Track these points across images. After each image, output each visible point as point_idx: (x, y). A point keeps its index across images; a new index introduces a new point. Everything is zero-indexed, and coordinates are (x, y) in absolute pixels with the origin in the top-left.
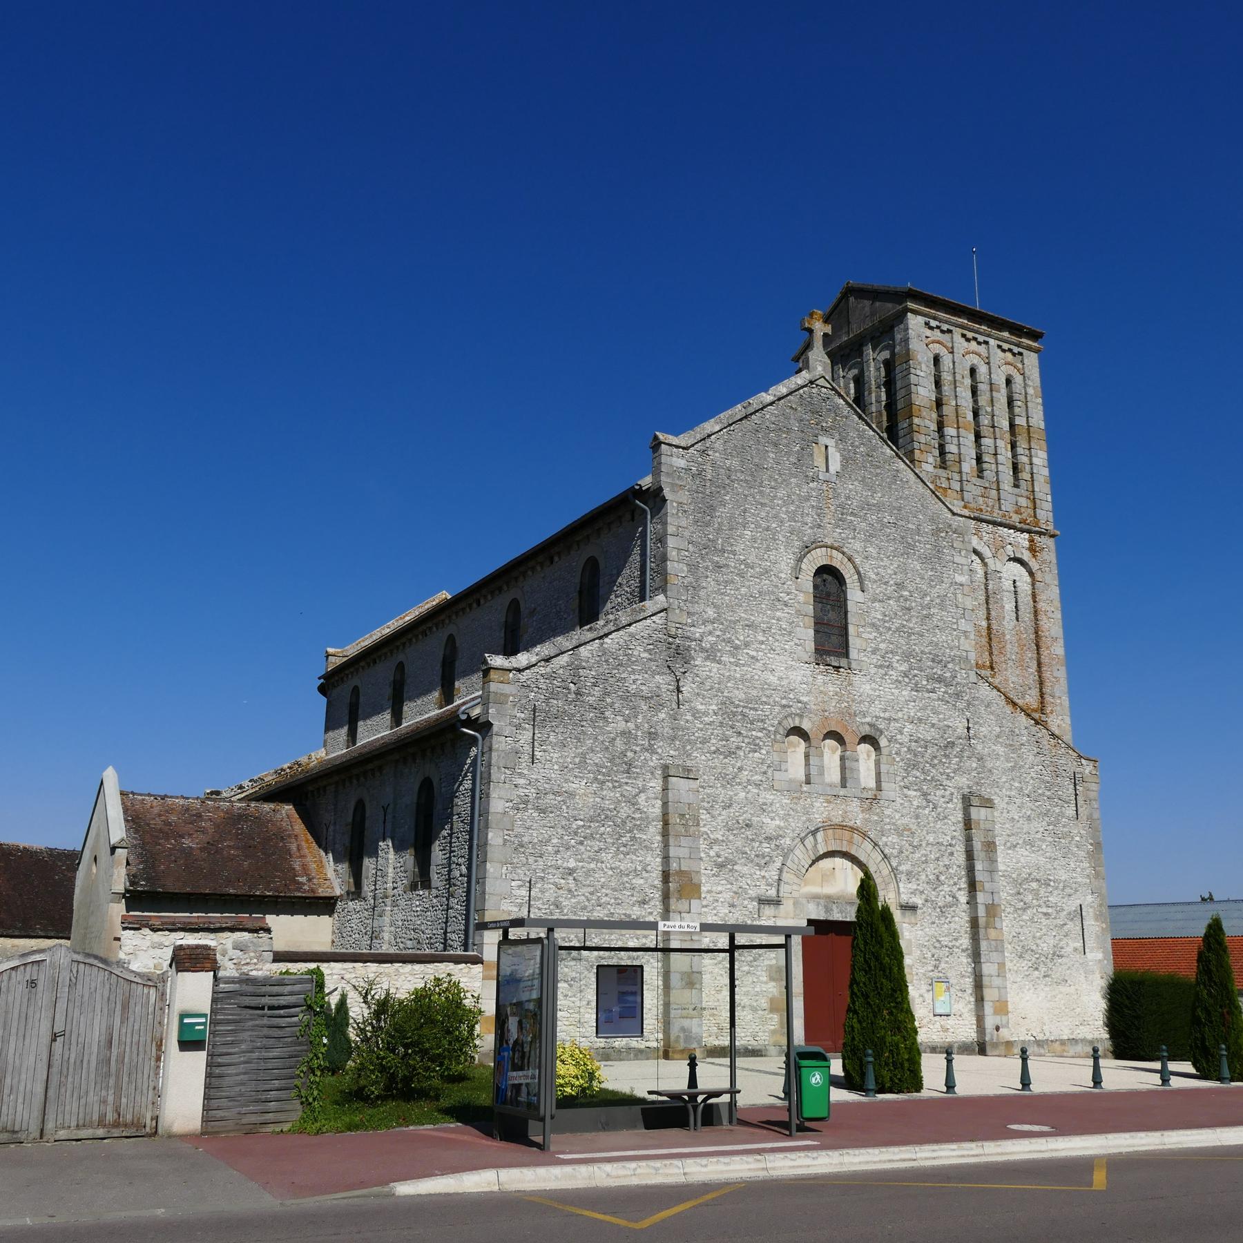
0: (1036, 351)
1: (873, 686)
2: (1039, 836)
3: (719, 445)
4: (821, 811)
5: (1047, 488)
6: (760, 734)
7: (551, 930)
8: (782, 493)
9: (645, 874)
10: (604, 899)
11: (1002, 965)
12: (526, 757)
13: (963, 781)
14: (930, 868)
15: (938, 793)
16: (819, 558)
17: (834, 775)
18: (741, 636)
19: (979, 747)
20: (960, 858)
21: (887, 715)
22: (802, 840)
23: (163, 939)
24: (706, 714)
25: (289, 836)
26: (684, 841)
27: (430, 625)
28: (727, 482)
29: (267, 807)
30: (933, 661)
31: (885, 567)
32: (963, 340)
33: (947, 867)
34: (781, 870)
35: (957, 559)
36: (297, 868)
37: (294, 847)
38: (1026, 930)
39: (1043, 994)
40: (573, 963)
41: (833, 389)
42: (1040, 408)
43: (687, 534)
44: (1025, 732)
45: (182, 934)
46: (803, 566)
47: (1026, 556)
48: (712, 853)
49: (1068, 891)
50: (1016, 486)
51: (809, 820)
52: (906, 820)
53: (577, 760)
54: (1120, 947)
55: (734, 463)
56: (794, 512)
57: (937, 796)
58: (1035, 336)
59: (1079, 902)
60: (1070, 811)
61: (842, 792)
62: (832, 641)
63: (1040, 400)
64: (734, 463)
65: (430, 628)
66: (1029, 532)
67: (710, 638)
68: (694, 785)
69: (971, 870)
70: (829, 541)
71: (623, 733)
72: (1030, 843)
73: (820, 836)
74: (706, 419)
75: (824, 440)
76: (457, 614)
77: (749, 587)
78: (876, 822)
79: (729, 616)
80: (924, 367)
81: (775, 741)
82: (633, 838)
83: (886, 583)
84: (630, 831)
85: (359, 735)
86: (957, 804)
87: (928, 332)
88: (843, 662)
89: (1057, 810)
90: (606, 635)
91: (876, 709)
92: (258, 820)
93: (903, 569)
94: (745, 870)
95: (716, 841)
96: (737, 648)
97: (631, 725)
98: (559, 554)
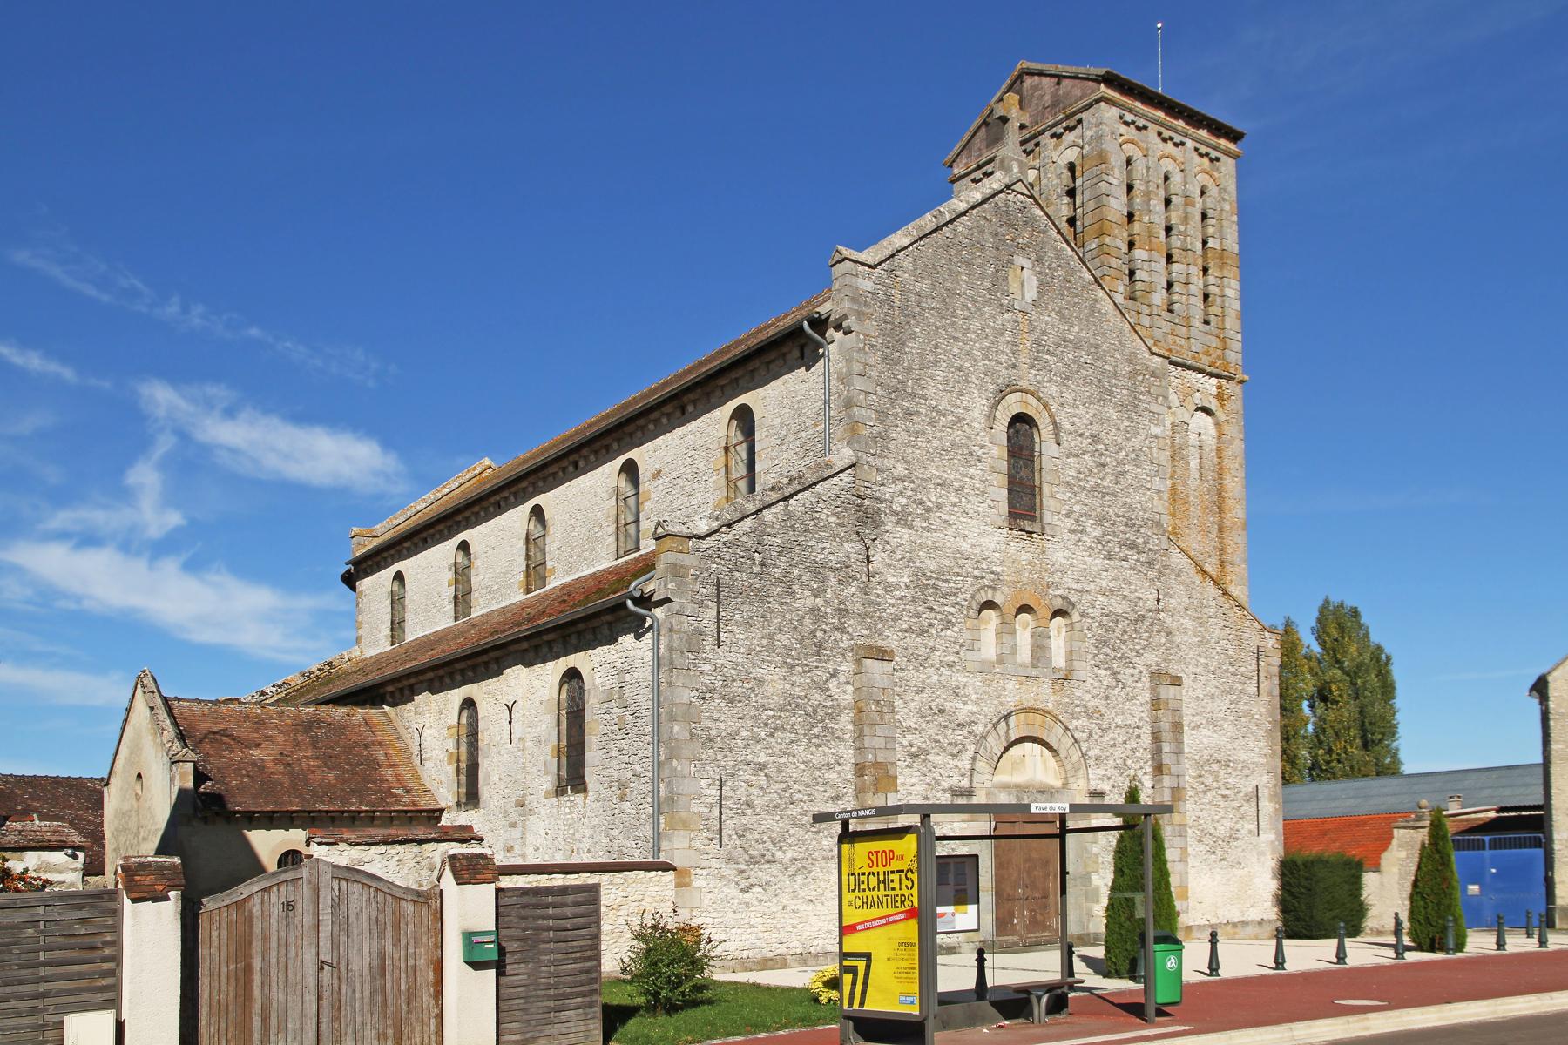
0: (1235, 157)
1: (1067, 555)
2: (1221, 715)
3: (908, 264)
4: (1013, 693)
5: (1237, 325)
6: (953, 610)
7: (925, 817)
8: (975, 325)
9: (838, 768)
10: (798, 796)
11: (1184, 850)
12: (710, 640)
13: (1151, 658)
14: (1118, 753)
15: (1128, 671)
16: (1014, 404)
17: (1024, 655)
18: (933, 496)
19: (1169, 620)
20: (1146, 740)
21: (1079, 587)
22: (995, 726)
23: (363, 854)
24: (897, 587)
25: (373, 743)
26: (880, 730)
27: (505, 494)
28: (917, 310)
29: (341, 711)
30: (1126, 525)
31: (1080, 416)
32: (1158, 140)
33: (1134, 750)
34: (973, 759)
35: (1153, 407)
36: (392, 779)
37: (381, 756)
38: (1205, 814)
39: (1218, 877)
40: (766, 866)
41: (1031, 196)
42: (1235, 227)
43: (875, 374)
44: (1213, 603)
45: (454, 844)
46: (998, 414)
47: (1213, 405)
48: (905, 743)
49: (1246, 772)
50: (1206, 322)
51: (1001, 704)
52: (1096, 702)
53: (765, 642)
54: (1292, 830)
55: (924, 286)
56: (988, 349)
57: (1126, 675)
58: (1235, 136)
59: (1254, 783)
60: (1252, 688)
61: (1034, 673)
62: (1023, 505)
63: (1235, 218)
64: (924, 286)
65: (506, 499)
66: (1218, 376)
67: (901, 499)
68: (888, 667)
69: (1157, 752)
70: (1024, 384)
71: (812, 610)
72: (1213, 723)
73: (1012, 720)
74: (893, 231)
75: (1020, 260)
76: (544, 479)
77: (940, 439)
78: (1068, 705)
79: (920, 473)
80: (1117, 173)
81: (967, 616)
82: (825, 729)
83: (1081, 435)
84: (822, 721)
85: (408, 625)
86: (1146, 682)
87: (1123, 129)
88: (1036, 527)
89: (1240, 687)
90: (791, 496)
91: (1068, 581)
92: (337, 729)
93: (1098, 418)
94: (937, 759)
95: (908, 729)
96: (928, 510)
97: (819, 602)
98: (694, 402)
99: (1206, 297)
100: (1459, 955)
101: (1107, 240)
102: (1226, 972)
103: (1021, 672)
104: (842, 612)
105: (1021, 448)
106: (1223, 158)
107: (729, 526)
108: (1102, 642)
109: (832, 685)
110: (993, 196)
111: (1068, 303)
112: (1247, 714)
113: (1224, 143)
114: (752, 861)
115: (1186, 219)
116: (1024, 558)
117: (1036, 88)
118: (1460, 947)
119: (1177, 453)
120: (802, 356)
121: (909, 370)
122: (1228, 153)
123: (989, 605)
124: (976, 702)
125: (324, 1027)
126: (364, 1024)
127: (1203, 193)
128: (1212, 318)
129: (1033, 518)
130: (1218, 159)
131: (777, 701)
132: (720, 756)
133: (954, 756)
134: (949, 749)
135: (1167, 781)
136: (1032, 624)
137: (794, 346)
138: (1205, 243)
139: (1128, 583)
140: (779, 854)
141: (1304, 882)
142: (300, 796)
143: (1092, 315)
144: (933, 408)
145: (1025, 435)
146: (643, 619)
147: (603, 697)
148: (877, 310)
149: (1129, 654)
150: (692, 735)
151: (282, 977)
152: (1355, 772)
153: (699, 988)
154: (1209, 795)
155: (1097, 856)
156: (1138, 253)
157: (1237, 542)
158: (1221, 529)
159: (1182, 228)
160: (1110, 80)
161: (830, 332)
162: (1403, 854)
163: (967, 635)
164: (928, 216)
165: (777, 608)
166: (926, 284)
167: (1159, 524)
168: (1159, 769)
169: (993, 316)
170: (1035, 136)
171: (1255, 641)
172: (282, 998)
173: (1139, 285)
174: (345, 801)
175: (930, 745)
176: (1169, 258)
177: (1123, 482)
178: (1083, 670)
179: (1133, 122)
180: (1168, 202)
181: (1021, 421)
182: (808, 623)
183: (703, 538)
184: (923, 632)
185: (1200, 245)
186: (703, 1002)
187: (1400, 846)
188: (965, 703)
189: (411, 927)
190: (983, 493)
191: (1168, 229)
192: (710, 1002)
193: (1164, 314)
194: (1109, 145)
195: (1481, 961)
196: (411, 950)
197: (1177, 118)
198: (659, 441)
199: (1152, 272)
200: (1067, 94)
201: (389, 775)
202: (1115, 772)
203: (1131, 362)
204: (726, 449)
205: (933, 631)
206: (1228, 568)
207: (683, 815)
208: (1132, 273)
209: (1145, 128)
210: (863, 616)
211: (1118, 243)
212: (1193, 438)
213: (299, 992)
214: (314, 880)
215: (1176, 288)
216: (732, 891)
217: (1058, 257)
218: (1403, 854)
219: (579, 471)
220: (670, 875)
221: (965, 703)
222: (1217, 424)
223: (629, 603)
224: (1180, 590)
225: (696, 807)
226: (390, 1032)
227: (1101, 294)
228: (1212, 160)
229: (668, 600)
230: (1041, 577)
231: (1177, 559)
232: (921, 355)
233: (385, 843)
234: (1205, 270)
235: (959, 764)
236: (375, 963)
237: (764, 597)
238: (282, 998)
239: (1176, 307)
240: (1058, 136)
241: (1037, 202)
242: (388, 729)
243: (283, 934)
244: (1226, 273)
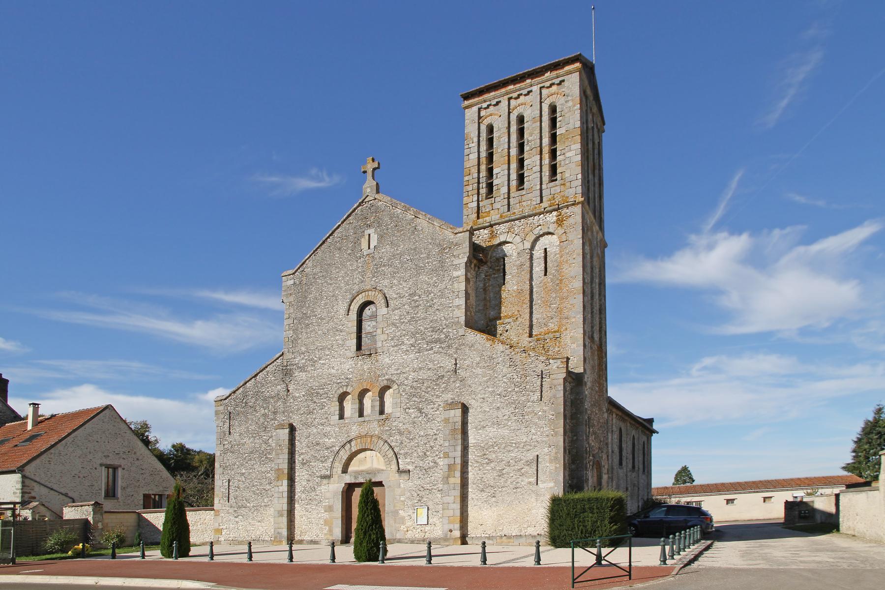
2: (506, 417)
21: (399, 371)
57: (428, 409)
70: (368, 287)
73: (353, 443)
95: (302, 454)
114: (239, 507)
139: (432, 361)
216: (232, 518)
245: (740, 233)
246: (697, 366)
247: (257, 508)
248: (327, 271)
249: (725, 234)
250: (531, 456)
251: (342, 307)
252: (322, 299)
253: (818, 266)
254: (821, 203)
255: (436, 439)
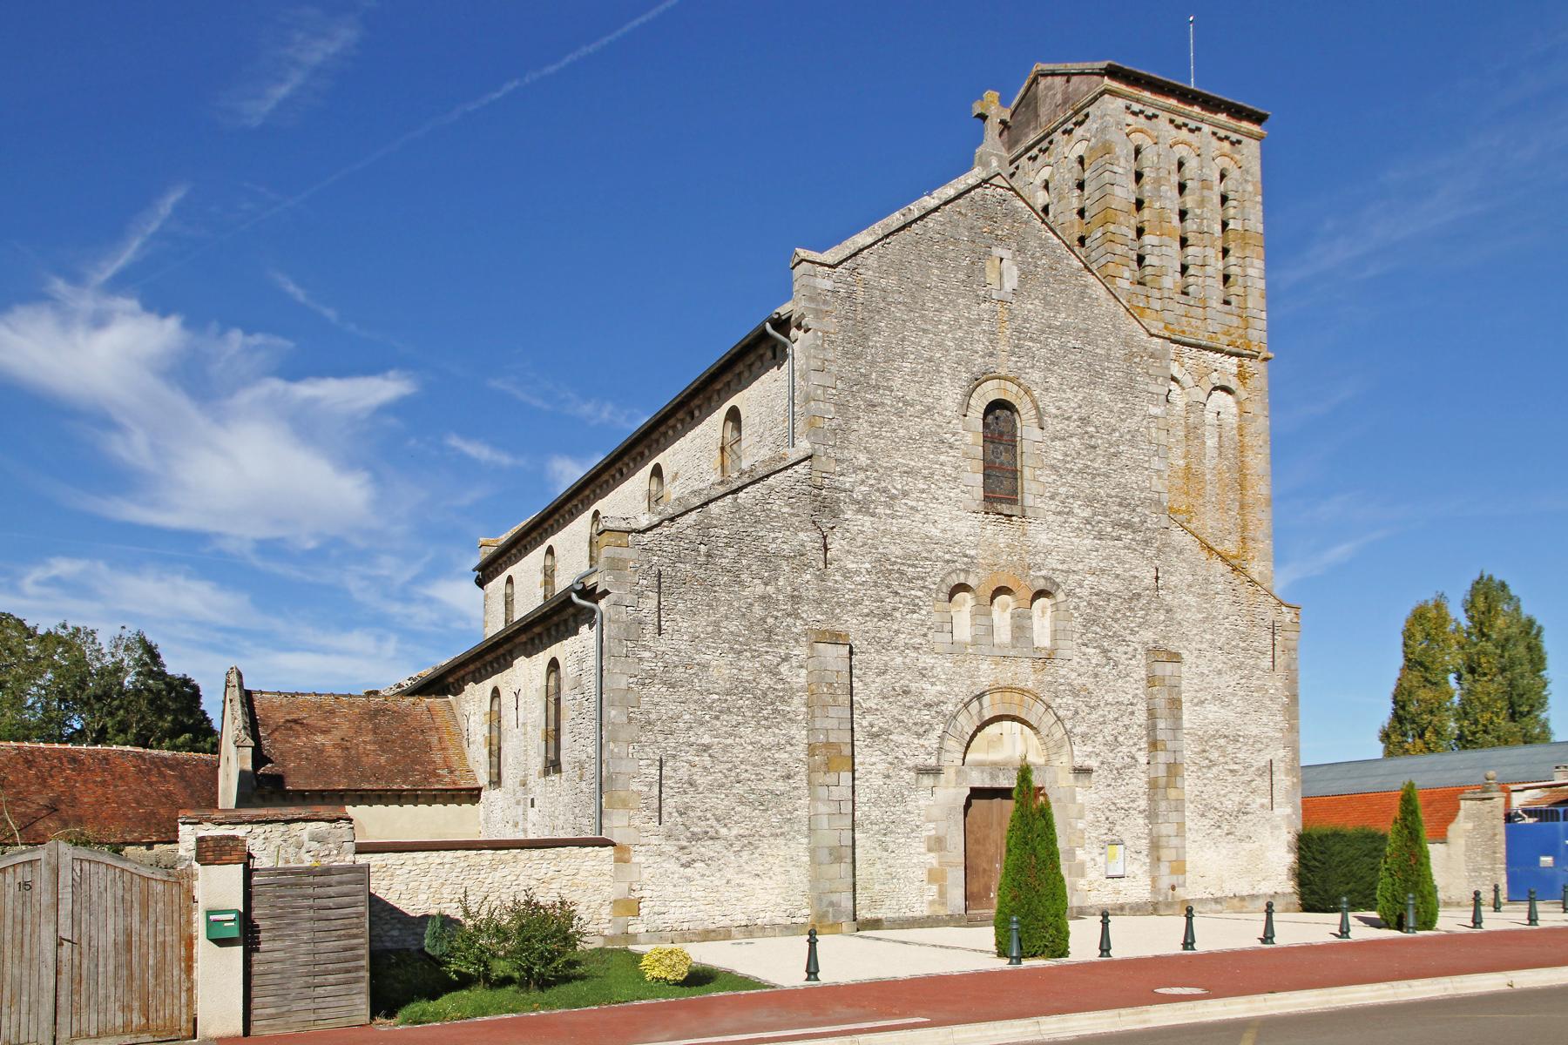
0: (1259, 138)
1: (1050, 535)
2: (1230, 690)
4: (987, 673)
6: (920, 594)
8: (948, 316)
9: (789, 748)
11: (1181, 825)
12: (650, 629)
13: (1148, 635)
15: (1120, 649)
16: (991, 391)
17: (1003, 633)
19: (1169, 598)
20: (1141, 717)
21: (1065, 567)
22: (966, 705)
24: (858, 573)
27: (575, 502)
30: (1120, 505)
31: (1068, 400)
32: (1171, 127)
33: (1127, 727)
36: (439, 761)
37: (434, 740)
38: (1210, 788)
39: (1224, 852)
41: (1012, 189)
42: (1259, 208)
43: (834, 369)
47: (1233, 383)
48: (865, 723)
49: (1258, 746)
50: (1227, 302)
52: (1083, 680)
53: (710, 629)
56: (962, 339)
57: (1119, 653)
58: (1258, 119)
59: (1268, 757)
60: (1266, 662)
62: (1001, 487)
63: (1259, 199)
66: (1238, 355)
67: (863, 488)
69: (1152, 728)
70: (1003, 372)
72: (1219, 699)
73: (986, 700)
75: (998, 251)
78: (1051, 683)
80: (1122, 161)
82: (776, 711)
83: (1068, 419)
86: (1141, 658)
87: (1130, 119)
88: (1016, 510)
89: (1252, 662)
90: (740, 489)
91: (1052, 562)
93: (1089, 401)
95: (869, 710)
96: (893, 497)
99: (1226, 278)
100: (1064, 960)
101: (1112, 228)
102: (1201, 946)
103: (997, 651)
104: (795, 599)
105: (1001, 434)
106: (1245, 140)
107: (672, 519)
108: (1090, 621)
109: (784, 668)
110: (968, 191)
111: (1053, 290)
112: (1260, 688)
113: (1246, 125)
114: (694, 837)
115: (1202, 203)
116: (1002, 541)
117: (1049, 88)
118: (1428, 924)
119: (1193, 432)
120: (774, 357)
121: (873, 363)
122: (1250, 135)
123: (962, 587)
124: (944, 682)
125: (62, 1000)
126: (107, 997)
127: (1223, 176)
128: (1233, 299)
129: (1014, 502)
130: (1239, 142)
131: (722, 685)
132: (660, 738)
133: (919, 736)
134: (914, 728)
135: (1162, 757)
136: (1013, 605)
137: (761, 349)
138: (1225, 225)
139: (1122, 562)
140: (724, 831)
141: (1319, 857)
142: (350, 777)
143: (1081, 299)
144: (899, 399)
145: (1006, 421)
146: (593, 611)
147: (572, 684)
148: (837, 307)
149: (1122, 632)
150: (630, 719)
151: (17, 953)
152: (1503, 741)
153: (572, 964)
154: (1215, 770)
155: (1082, 831)
156: (1147, 239)
157: (1261, 521)
158: (1242, 507)
159: (1198, 211)
160: (1113, 72)
161: (794, 332)
162: (1470, 826)
163: (936, 618)
164: (897, 214)
165: (723, 596)
166: (892, 281)
167: (1159, 503)
168: (1154, 745)
169: (968, 308)
170: (1048, 135)
171: (1271, 615)
172: (16, 972)
173: (1148, 270)
174: (391, 780)
175: (893, 725)
176: (1184, 242)
177: (1116, 463)
178: (1068, 648)
179: (1142, 112)
180: (1182, 187)
181: (998, 407)
182: (758, 610)
183: (644, 531)
184: (886, 616)
185: (1218, 228)
186: (575, 978)
187: (1467, 817)
188: (933, 684)
189: (160, 905)
190: (955, 479)
191: (1183, 214)
192: (582, 977)
193: (1178, 297)
194: (1115, 136)
195: (1451, 939)
196: (160, 927)
197: (1191, 105)
198: (676, 445)
199: (1164, 255)
200: (1075, 90)
201: (438, 757)
202: (1105, 748)
203: (1126, 344)
204: (723, 449)
205: (897, 614)
206: (1251, 544)
207: (623, 794)
208: (1141, 259)
209: (1155, 116)
210: (819, 602)
211: (1124, 230)
212: (1210, 417)
213: (35, 968)
214: (53, 861)
215: (1191, 271)
216: (672, 866)
217: (1042, 246)
218: (1470, 826)
219: (624, 477)
220: (609, 851)
221: (933, 684)
222: (1238, 403)
223: (574, 596)
224: (1183, 567)
225: (635, 786)
226: (136, 1004)
227: (1092, 279)
228: (1233, 143)
229: (606, 593)
230: (1021, 559)
231: (1178, 536)
232: (886, 349)
233: (250, 822)
234: (1225, 252)
235: (926, 743)
236: (121, 939)
237: (710, 587)
238: (16, 972)
239: (1191, 289)
240: (1068, 132)
241: (1018, 194)
242: (448, 716)
243: (19, 912)
244: (1247, 253)
245: (164, 314)
246: (38, 573)
247: (749, 842)
248: (912, 296)
249: (133, 304)
250: (1262, 761)
251: (950, 396)
252: (903, 356)
253: (306, 427)
254: (330, 313)
255: (1132, 713)
